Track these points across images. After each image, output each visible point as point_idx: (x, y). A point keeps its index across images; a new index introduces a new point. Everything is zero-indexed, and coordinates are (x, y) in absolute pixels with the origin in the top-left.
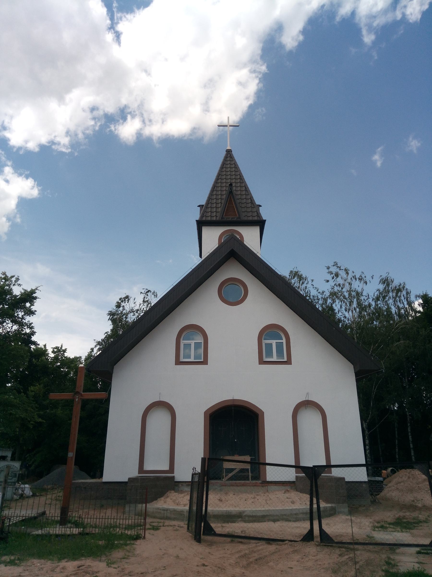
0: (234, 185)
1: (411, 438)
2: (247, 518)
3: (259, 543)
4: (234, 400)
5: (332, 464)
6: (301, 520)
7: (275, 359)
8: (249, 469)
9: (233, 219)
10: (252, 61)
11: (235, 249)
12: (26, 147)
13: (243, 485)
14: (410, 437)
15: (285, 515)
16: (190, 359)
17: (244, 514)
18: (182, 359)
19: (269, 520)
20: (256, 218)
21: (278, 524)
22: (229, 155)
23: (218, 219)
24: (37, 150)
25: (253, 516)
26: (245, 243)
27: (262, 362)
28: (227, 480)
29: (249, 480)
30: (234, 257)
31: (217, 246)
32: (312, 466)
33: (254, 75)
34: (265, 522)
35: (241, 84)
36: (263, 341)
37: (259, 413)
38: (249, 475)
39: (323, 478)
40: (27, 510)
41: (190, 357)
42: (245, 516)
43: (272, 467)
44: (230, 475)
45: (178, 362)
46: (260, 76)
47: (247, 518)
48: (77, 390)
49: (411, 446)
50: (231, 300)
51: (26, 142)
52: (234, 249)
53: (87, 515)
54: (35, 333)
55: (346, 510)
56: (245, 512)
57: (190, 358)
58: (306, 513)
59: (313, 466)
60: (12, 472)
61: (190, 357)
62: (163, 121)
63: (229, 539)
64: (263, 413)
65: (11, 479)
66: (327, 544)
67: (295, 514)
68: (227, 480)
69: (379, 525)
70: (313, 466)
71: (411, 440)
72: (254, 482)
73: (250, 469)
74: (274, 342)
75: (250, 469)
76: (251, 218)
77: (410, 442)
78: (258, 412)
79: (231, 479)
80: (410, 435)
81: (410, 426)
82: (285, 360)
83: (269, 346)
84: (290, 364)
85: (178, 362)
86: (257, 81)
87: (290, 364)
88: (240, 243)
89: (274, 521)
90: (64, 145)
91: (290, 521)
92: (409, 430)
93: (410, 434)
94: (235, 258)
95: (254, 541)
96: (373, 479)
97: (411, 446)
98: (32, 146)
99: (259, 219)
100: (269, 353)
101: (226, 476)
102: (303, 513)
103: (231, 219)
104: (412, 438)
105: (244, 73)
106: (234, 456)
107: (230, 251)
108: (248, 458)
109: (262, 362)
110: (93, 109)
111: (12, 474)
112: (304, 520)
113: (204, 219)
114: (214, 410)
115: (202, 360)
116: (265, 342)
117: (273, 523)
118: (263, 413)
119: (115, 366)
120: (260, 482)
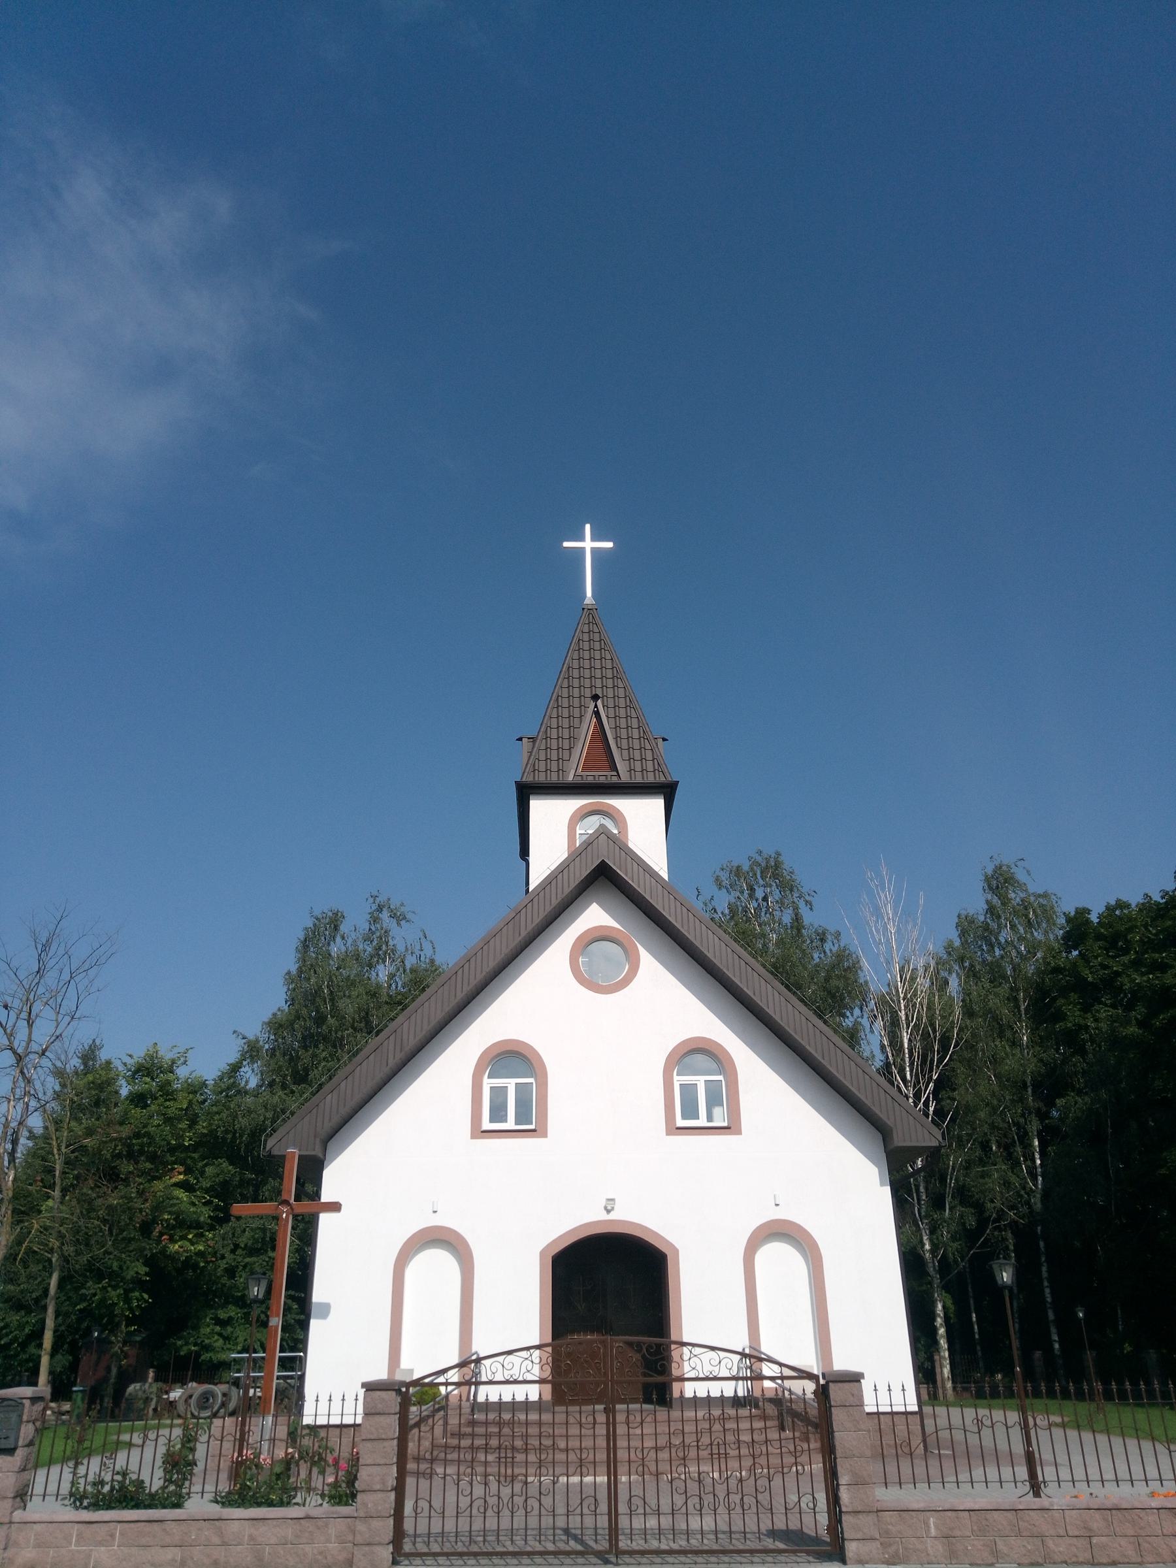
1: (1048, 1295)
14: (1047, 1291)
26: (631, 845)
31: (566, 855)
36: (676, 1078)
37: (666, 1252)
48: (284, 1196)
49: (1051, 1315)
54: (364, 1385)
69: (409, 946)
71: (1049, 1300)
77: (1048, 1306)
80: (1047, 1287)
81: (1045, 1264)
84: (738, 1132)
87: (738, 1132)
88: (619, 844)
92: (1045, 1274)
93: (1046, 1284)
97: (1051, 1315)
99: (663, 779)
100: (690, 1110)
104: (1052, 1293)
109: (673, 1129)
110: (951, 941)
115: (532, 1127)
118: (677, 1251)
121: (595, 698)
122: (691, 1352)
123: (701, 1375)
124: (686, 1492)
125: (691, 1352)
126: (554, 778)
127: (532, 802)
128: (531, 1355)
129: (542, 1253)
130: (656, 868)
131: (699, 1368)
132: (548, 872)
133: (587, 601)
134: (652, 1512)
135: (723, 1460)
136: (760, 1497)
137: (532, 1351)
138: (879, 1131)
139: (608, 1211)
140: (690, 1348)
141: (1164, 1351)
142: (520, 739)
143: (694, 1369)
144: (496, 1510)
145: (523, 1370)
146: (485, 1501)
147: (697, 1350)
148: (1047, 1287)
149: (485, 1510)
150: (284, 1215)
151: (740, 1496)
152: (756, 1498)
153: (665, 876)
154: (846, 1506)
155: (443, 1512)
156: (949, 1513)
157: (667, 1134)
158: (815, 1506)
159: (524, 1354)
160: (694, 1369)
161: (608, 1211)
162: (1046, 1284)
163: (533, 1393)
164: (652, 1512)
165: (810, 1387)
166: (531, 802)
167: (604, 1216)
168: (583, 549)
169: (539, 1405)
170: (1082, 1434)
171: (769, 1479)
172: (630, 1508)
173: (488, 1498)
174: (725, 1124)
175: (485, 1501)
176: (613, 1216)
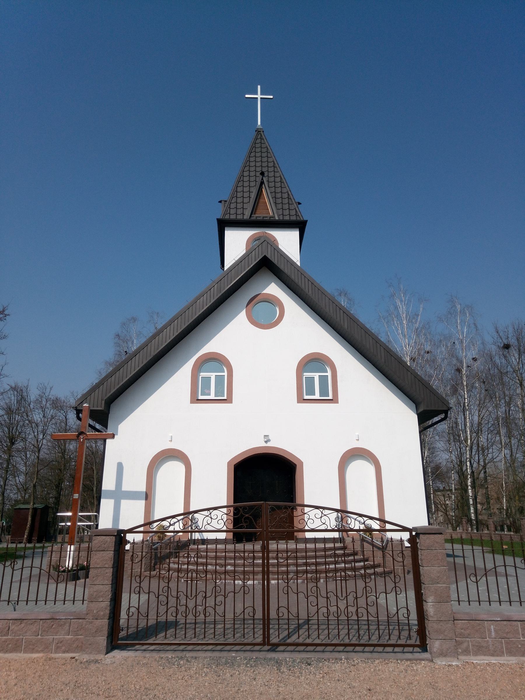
0: (266, 174)
1: (471, 493)
7: (317, 396)
11: (269, 256)
20: (294, 218)
22: (259, 136)
23: (245, 217)
26: (280, 247)
27: (301, 400)
30: (266, 267)
31: (244, 252)
32: (412, 528)
41: (209, 394)
50: (262, 322)
53: (454, 586)
57: (210, 395)
59: (413, 527)
61: (209, 394)
64: (302, 463)
70: (413, 527)
74: (316, 376)
78: (295, 462)
82: (330, 397)
83: (311, 381)
84: (337, 402)
85: (195, 400)
87: (337, 402)
94: (268, 268)
103: (268, 219)
109: (301, 400)
113: (227, 217)
115: (225, 398)
116: (307, 374)
121: (262, 174)
122: (322, 513)
123: (329, 528)
124: (317, 605)
125: (322, 513)
126: (239, 217)
127: (226, 232)
128: (210, 514)
129: (229, 463)
130: (295, 261)
131: (328, 523)
132: (234, 261)
133: (258, 127)
134: (293, 618)
135: (344, 582)
136: (370, 609)
137: (211, 511)
138: (414, 403)
139: (266, 442)
140: (321, 510)
141: (122, 535)
142: (220, 202)
143: (324, 524)
144: (184, 615)
145: (205, 523)
146: (177, 609)
147: (326, 512)
148: (470, 489)
149: (177, 615)
150: (82, 440)
151: (355, 608)
152: (367, 610)
153: (299, 264)
154: (432, 617)
155: (147, 616)
156: (505, 623)
157: (298, 403)
158: (408, 616)
159: (206, 513)
160: (324, 524)
161: (266, 442)
162: (469, 488)
163: (222, 536)
164: (293, 618)
165: (406, 536)
166: (226, 232)
167: (264, 445)
168: (257, 94)
169: (225, 541)
170: (506, 557)
171: (376, 597)
172: (278, 615)
173: (179, 607)
174: (332, 399)
175: (177, 609)
176: (269, 444)
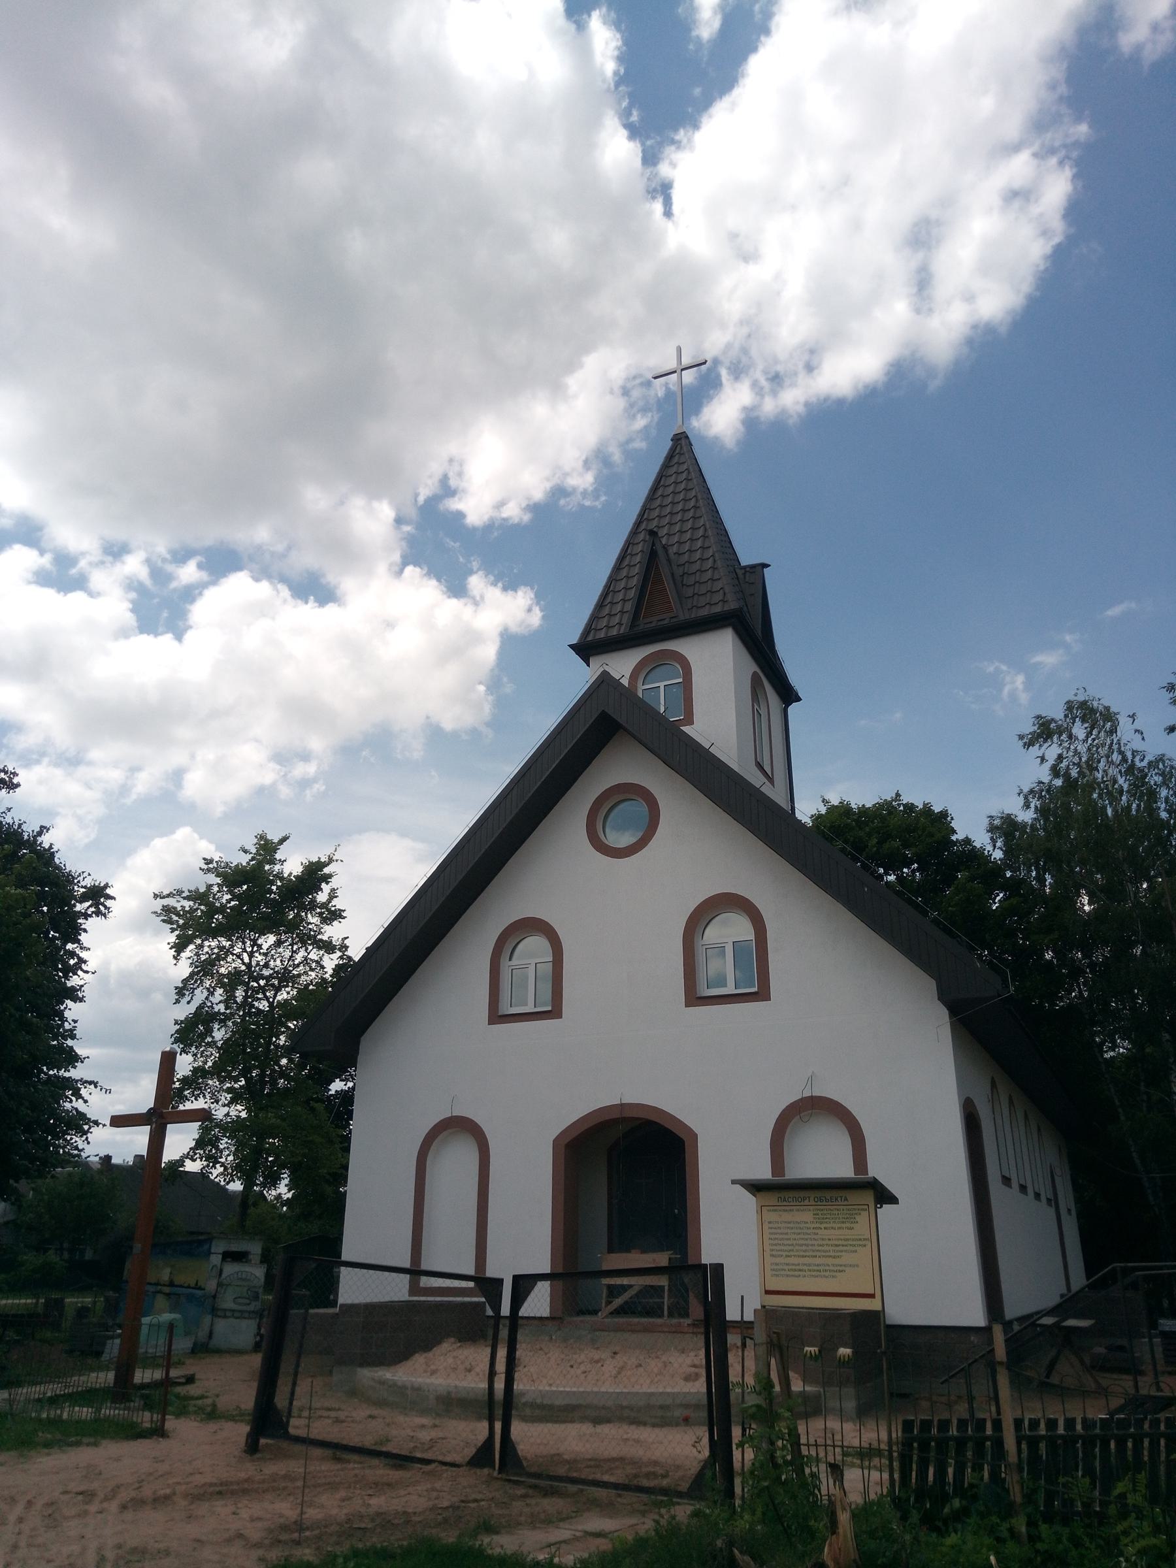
2: (528, 1412)
3: (447, 1470)
4: (622, 1106)
5: (424, 1266)
6: (677, 1425)
8: (664, 1286)
9: (662, 623)
10: (1041, 123)
12: (505, 520)
13: (647, 1330)
15: (631, 1408)
16: (526, 1007)
17: (523, 1400)
18: (506, 1009)
19: (584, 1419)
21: (606, 1429)
24: (527, 518)
25: (542, 1407)
28: (606, 1317)
29: (661, 1316)
33: (1053, 161)
34: (572, 1421)
35: (1018, 196)
38: (663, 1303)
39: (800, 1312)
40: (296, 1374)
42: (525, 1404)
43: (386, 1274)
44: (618, 1302)
45: (497, 1017)
46: (1075, 154)
47: (528, 1412)
51: (500, 505)
52: (606, 710)
55: (850, 1405)
56: (524, 1394)
58: (697, 1407)
60: (249, 1289)
62: (810, 368)
63: (328, 1452)
65: (249, 1304)
66: (515, 1478)
67: (661, 1407)
68: (606, 1317)
72: (674, 1321)
73: (666, 1288)
75: (666, 1288)
76: (704, 612)
79: (619, 1312)
85: (497, 1017)
86: (1068, 172)
89: (597, 1421)
90: (585, 493)
91: (645, 1424)
95: (355, 1457)
96: (666, 1313)
98: (513, 511)
101: (609, 1303)
102: (686, 1406)
105: (1020, 166)
106: (630, 1252)
107: (601, 714)
108: (662, 1259)
111: (249, 1292)
112: (686, 1421)
113: (590, 638)
114: (575, 1134)
117: (590, 1425)
118: (696, 1135)
119: (362, 1038)
120: (689, 1321)
